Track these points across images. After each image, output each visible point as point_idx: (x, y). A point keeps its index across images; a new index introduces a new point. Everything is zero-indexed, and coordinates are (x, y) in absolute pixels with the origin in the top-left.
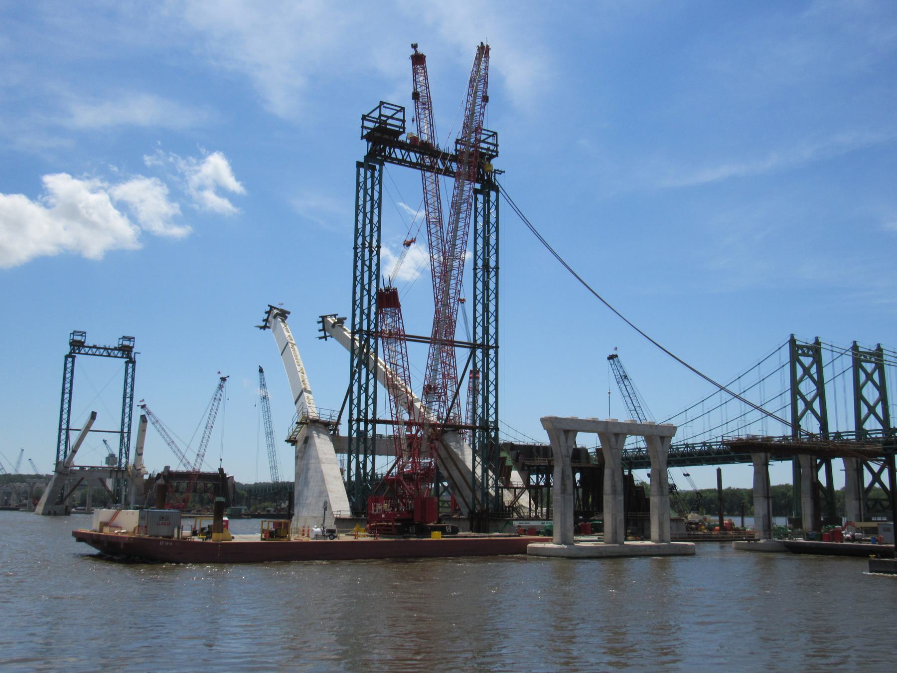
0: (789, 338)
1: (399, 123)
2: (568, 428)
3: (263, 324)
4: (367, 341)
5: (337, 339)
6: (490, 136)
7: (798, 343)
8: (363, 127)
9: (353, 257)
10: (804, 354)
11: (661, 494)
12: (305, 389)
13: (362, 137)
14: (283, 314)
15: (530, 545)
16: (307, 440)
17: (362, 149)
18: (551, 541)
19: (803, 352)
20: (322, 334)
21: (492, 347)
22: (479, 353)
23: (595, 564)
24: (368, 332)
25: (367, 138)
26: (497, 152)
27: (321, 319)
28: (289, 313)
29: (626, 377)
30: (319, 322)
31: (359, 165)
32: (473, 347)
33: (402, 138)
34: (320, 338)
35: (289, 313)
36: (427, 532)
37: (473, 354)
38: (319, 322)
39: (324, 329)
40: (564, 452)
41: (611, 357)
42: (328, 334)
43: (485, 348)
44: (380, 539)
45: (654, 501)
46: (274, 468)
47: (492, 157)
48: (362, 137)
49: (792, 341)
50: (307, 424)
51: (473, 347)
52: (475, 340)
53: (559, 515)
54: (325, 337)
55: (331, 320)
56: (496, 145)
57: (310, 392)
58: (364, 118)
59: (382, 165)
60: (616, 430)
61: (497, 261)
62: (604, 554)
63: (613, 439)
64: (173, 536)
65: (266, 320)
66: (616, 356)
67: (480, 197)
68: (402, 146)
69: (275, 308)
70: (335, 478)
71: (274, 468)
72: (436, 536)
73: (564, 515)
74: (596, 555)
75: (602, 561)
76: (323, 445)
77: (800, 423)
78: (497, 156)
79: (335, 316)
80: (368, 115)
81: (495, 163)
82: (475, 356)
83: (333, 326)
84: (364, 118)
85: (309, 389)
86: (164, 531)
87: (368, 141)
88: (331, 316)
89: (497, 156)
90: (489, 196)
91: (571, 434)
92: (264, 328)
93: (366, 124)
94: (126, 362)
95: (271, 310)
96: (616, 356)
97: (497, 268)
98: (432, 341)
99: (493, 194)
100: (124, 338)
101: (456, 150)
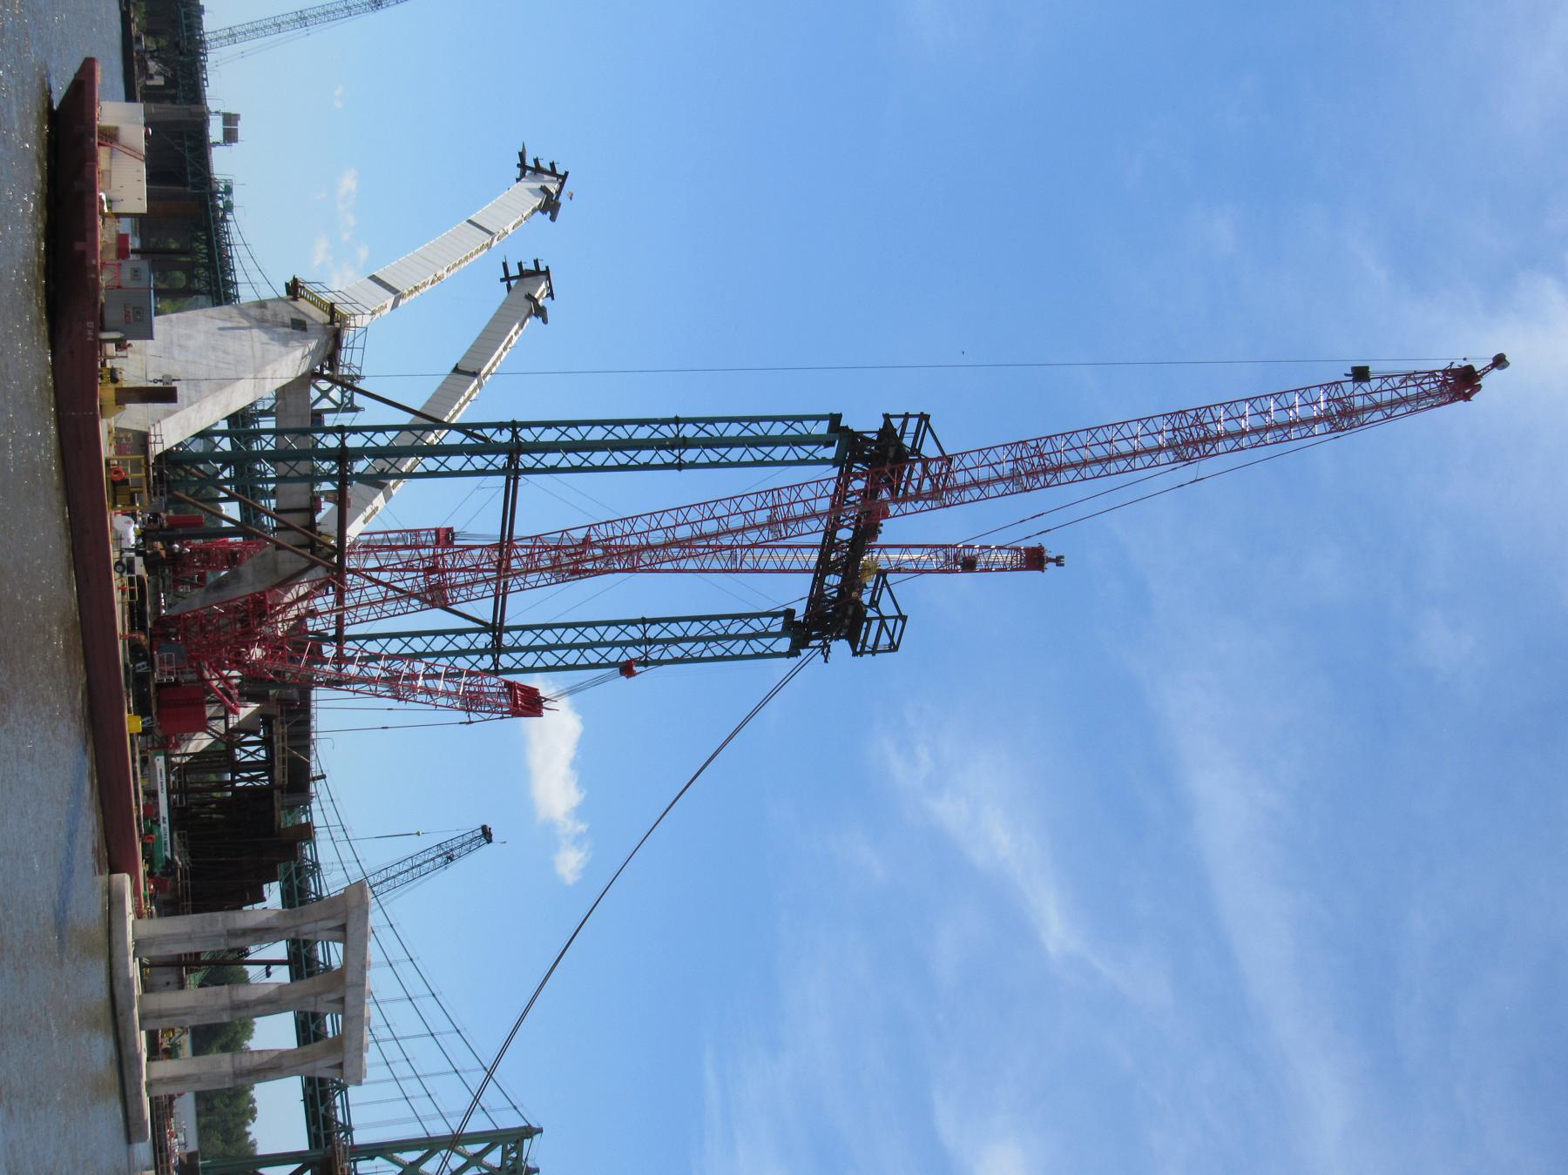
0: (534, 1125)
1: (870, 642)
2: (350, 930)
3: (530, 163)
4: (497, 449)
5: (504, 306)
6: (891, 637)
7: (527, 1142)
8: (907, 416)
9: (659, 416)
10: (505, 1154)
11: (238, 1074)
12: (402, 296)
13: (887, 417)
14: (550, 206)
15: (127, 877)
16: (299, 325)
17: (865, 421)
18: (139, 914)
19: (509, 1152)
20: (514, 271)
21: (515, 434)
22: (484, 640)
23: (105, 994)
24: (497, 649)
25: (887, 432)
26: (862, 653)
27: (542, 268)
28: (553, 219)
29: (451, 858)
30: (536, 262)
31: (835, 419)
32: (496, 628)
33: (885, 495)
34: (522, 156)
35: (553, 219)
36: (142, 709)
37: (486, 628)
38: (536, 262)
39: (524, 274)
40: (306, 928)
41: (486, 834)
42: (513, 283)
43: (515, 449)
44: (117, 595)
45: (221, 921)
46: (232, 36)
47: (853, 646)
48: (887, 417)
49: (529, 1132)
50: (332, 322)
51: (496, 628)
52: (509, 629)
53: (188, 929)
54: (507, 278)
55: (540, 291)
56: (874, 651)
57: (395, 305)
58: (924, 418)
59: (835, 462)
60: (349, 1000)
61: (693, 465)
62: (120, 1019)
63: (333, 996)
64: (103, 329)
65: (538, 170)
66: (490, 841)
67: (822, 428)
68: (869, 494)
69: (562, 185)
70: (228, 405)
71: (232, 36)
72: (133, 724)
73: (190, 938)
74: (119, 1009)
75: (108, 1004)
76: (290, 362)
77: (378, 1159)
78: (855, 654)
79: (551, 295)
80: (928, 425)
81: (840, 647)
82: (479, 631)
83: (530, 298)
84: (924, 418)
85: (401, 302)
86: (113, 315)
87: (880, 433)
88: (550, 287)
89: (855, 654)
90: (829, 444)
91: (338, 934)
92: (523, 166)
93: (912, 424)
94: (789, 614)
95: (559, 176)
96: (490, 841)
97: (680, 466)
98: (513, 473)
99: (784, 644)
100: (230, 120)
101: (866, 569)
